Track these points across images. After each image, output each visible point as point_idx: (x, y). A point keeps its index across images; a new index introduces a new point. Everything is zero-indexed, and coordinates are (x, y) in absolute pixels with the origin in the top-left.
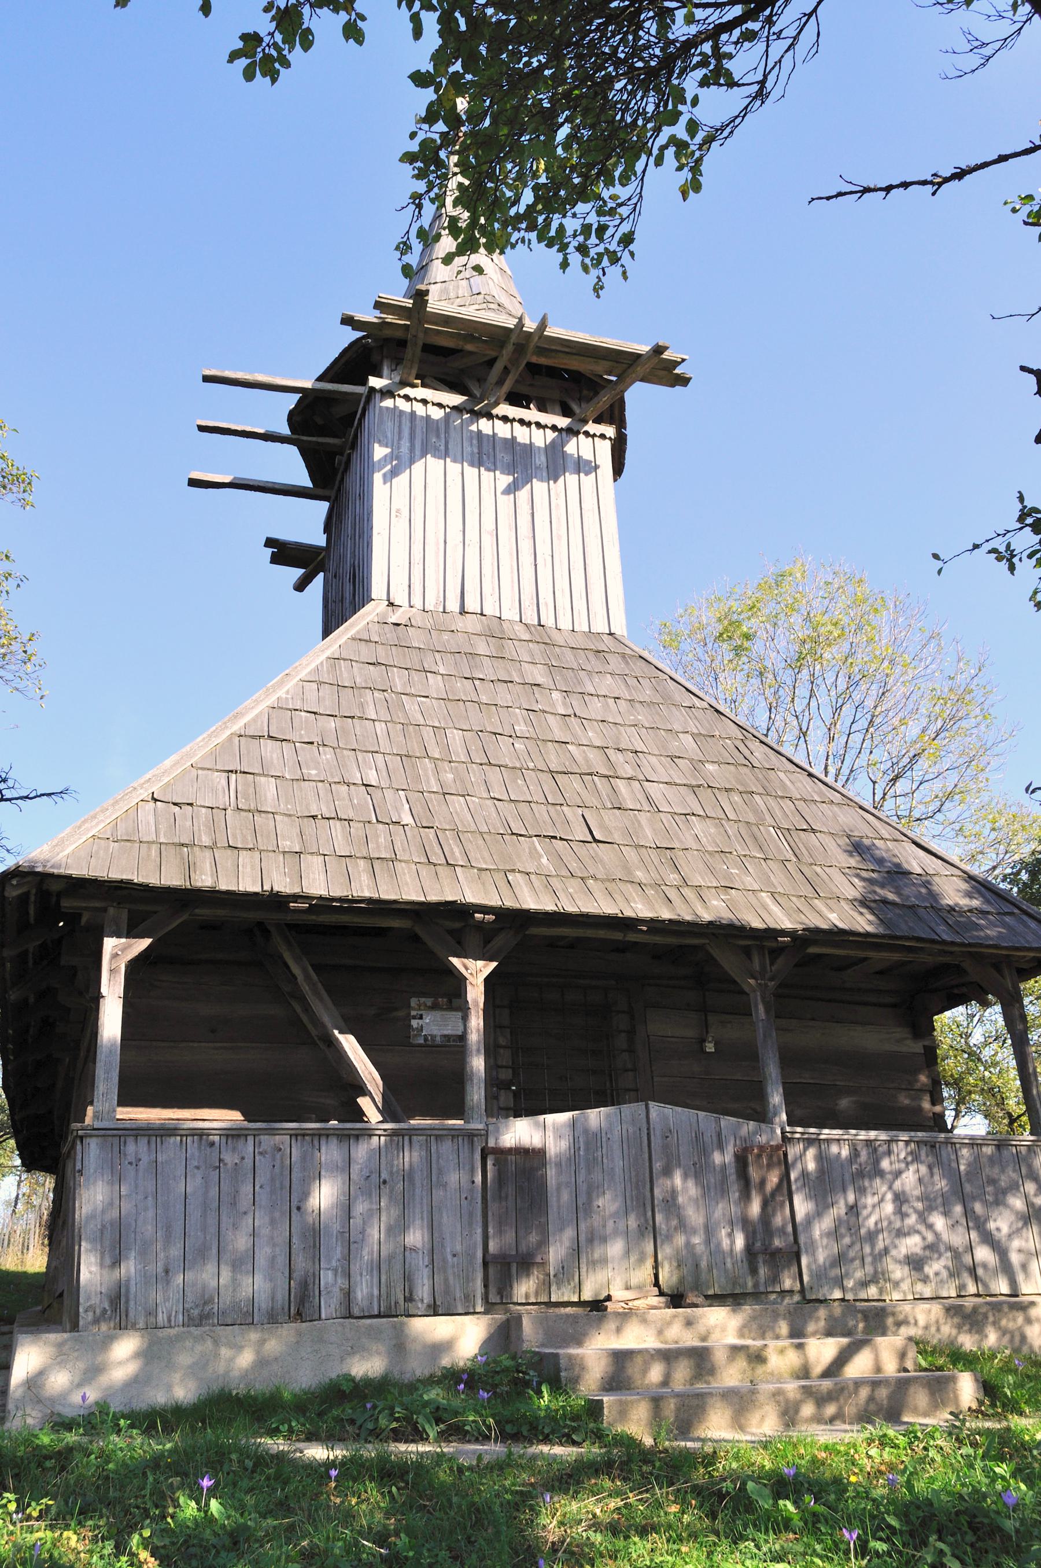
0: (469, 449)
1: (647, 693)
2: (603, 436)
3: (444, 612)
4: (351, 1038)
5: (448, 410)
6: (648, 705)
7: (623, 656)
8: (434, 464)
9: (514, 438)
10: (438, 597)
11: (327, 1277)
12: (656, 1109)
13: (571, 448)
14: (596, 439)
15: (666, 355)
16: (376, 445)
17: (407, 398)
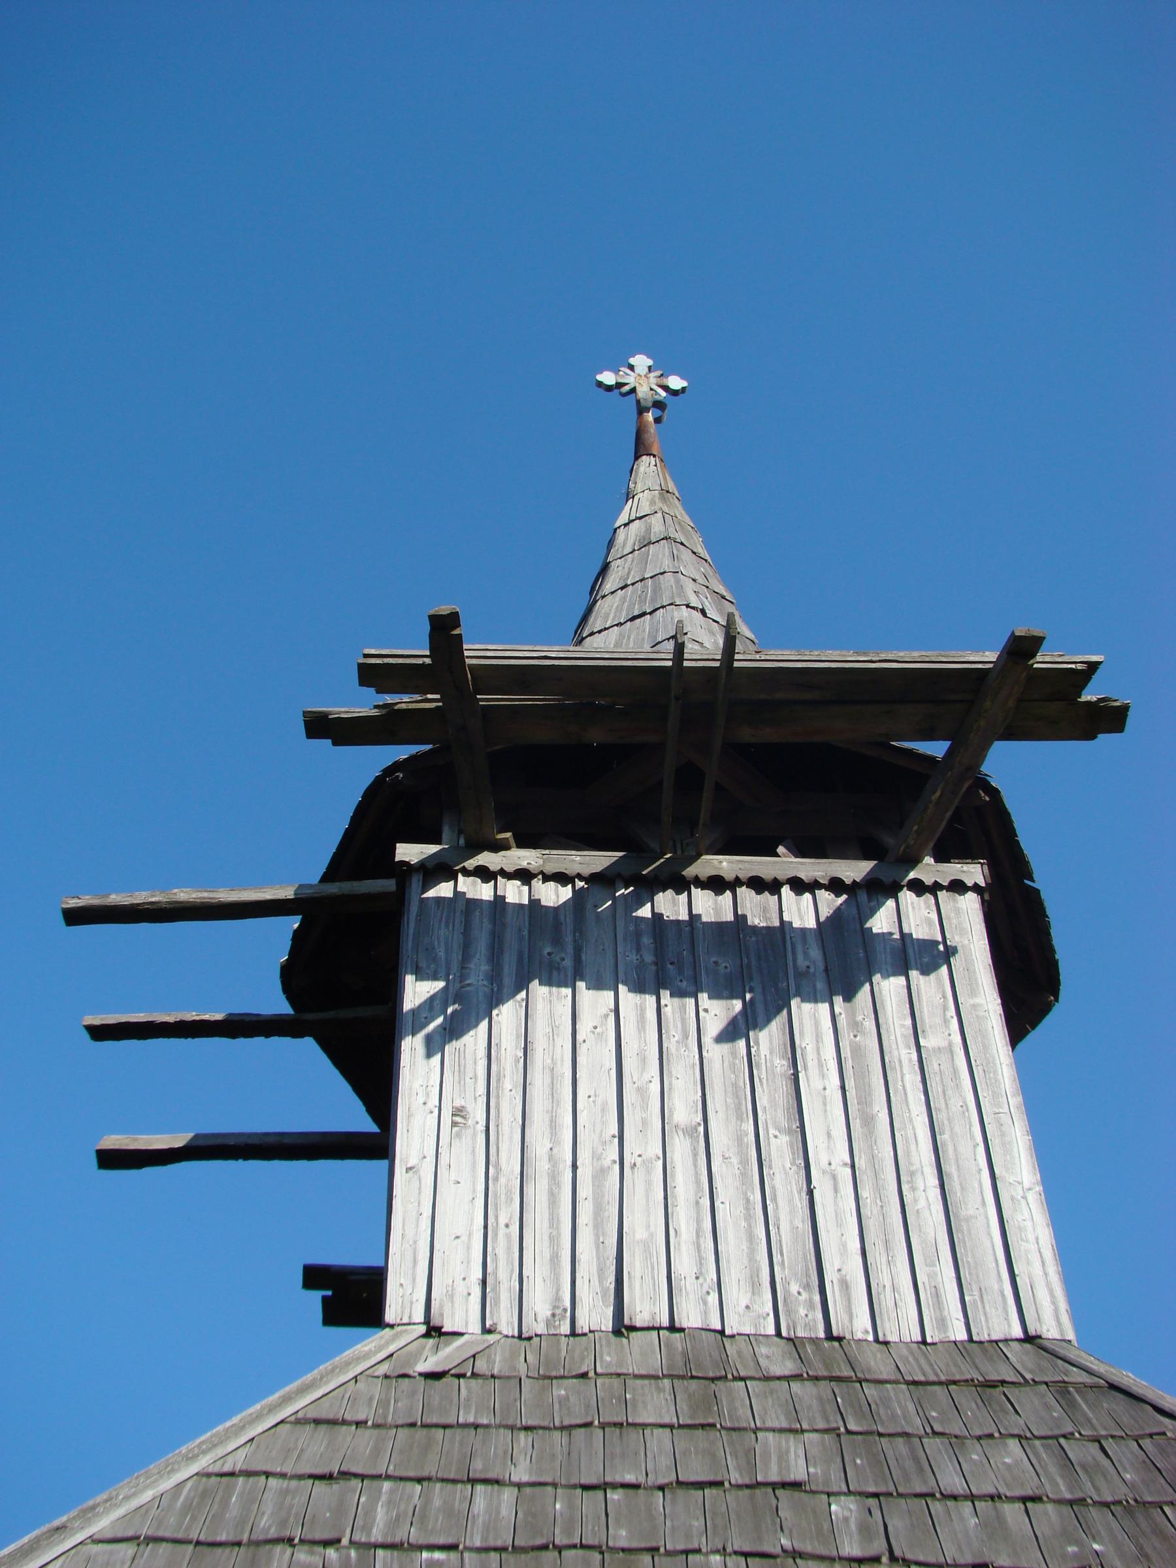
0: (633, 957)
2: (958, 887)
3: (573, 1334)
5: (580, 884)
6: (1128, 1509)
7: (1062, 1389)
8: (539, 991)
9: (740, 919)
10: (558, 1298)
13: (882, 922)
14: (942, 895)
15: (1043, 660)
16: (409, 979)
17: (485, 874)
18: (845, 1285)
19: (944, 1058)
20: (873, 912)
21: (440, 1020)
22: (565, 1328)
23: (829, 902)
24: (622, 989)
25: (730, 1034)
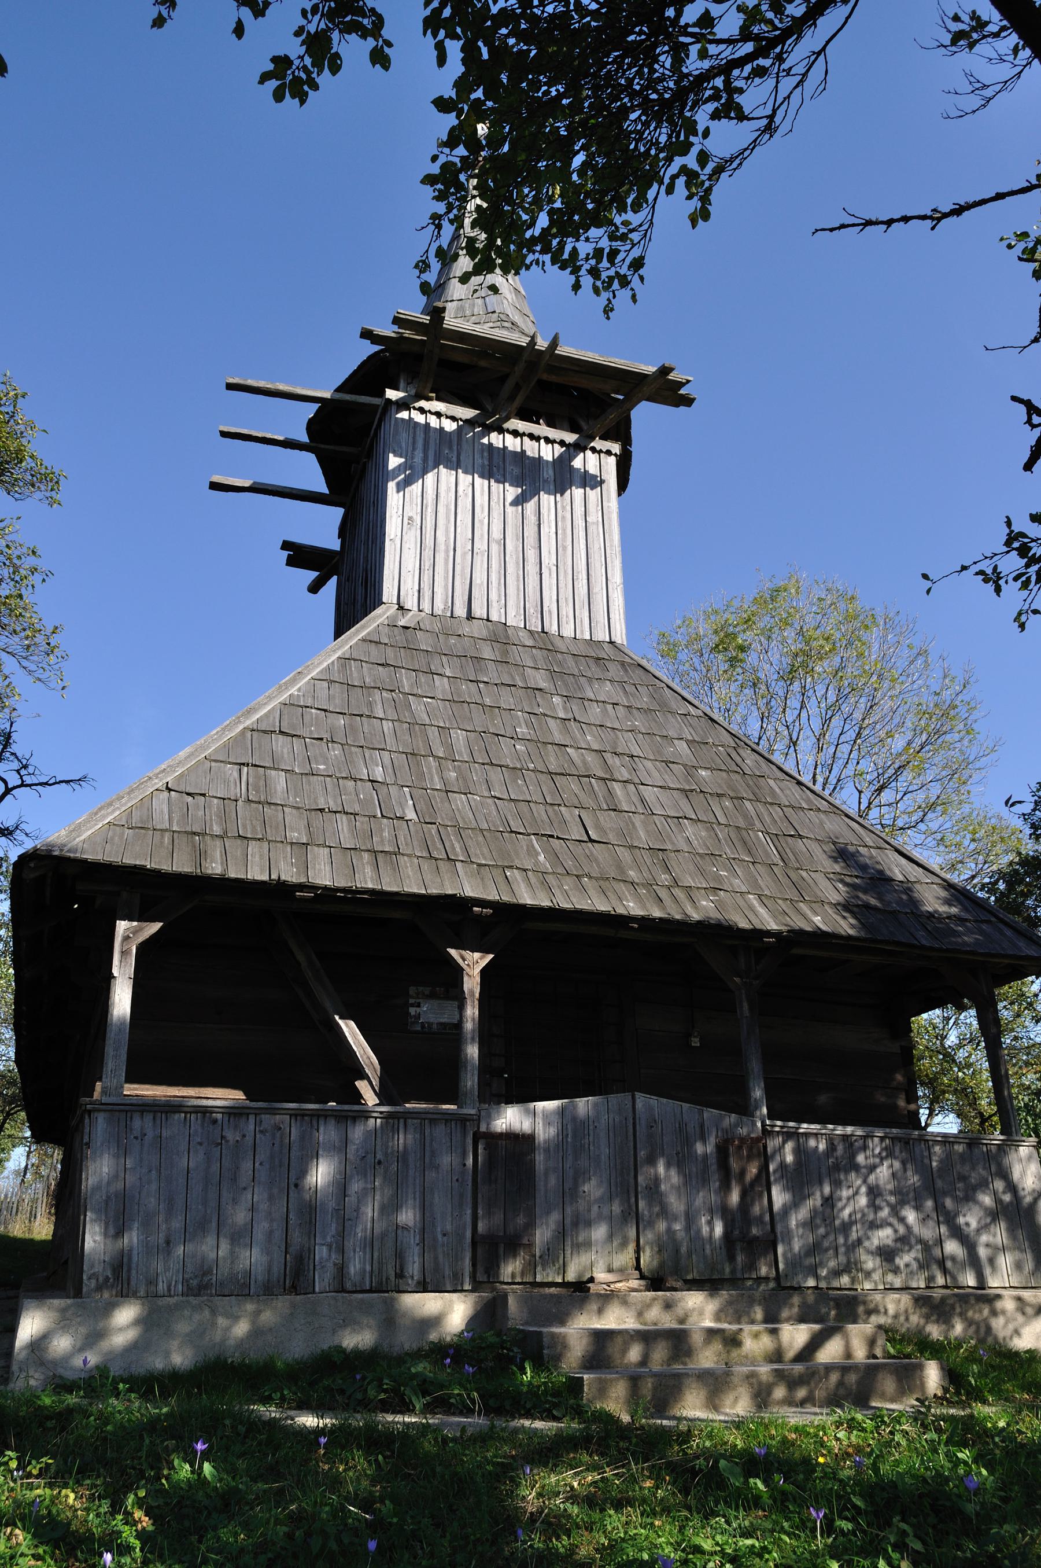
1: (644, 700)
2: (609, 453)
3: (452, 617)
4: (352, 1023)
5: (461, 423)
6: (645, 711)
7: (623, 664)
9: (523, 452)
11: (321, 1252)
12: (642, 1100)
14: (602, 455)
15: (671, 377)
17: (422, 410)
18: (550, 612)
19: (595, 527)
20: (575, 457)
21: (403, 476)
22: (449, 614)
23: (559, 450)
24: (476, 476)
25: (516, 502)
